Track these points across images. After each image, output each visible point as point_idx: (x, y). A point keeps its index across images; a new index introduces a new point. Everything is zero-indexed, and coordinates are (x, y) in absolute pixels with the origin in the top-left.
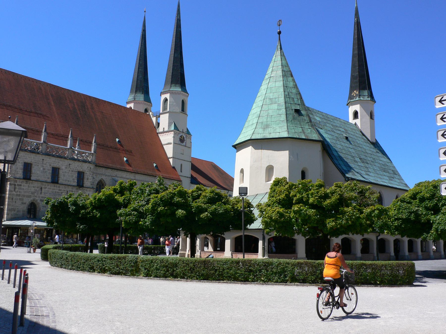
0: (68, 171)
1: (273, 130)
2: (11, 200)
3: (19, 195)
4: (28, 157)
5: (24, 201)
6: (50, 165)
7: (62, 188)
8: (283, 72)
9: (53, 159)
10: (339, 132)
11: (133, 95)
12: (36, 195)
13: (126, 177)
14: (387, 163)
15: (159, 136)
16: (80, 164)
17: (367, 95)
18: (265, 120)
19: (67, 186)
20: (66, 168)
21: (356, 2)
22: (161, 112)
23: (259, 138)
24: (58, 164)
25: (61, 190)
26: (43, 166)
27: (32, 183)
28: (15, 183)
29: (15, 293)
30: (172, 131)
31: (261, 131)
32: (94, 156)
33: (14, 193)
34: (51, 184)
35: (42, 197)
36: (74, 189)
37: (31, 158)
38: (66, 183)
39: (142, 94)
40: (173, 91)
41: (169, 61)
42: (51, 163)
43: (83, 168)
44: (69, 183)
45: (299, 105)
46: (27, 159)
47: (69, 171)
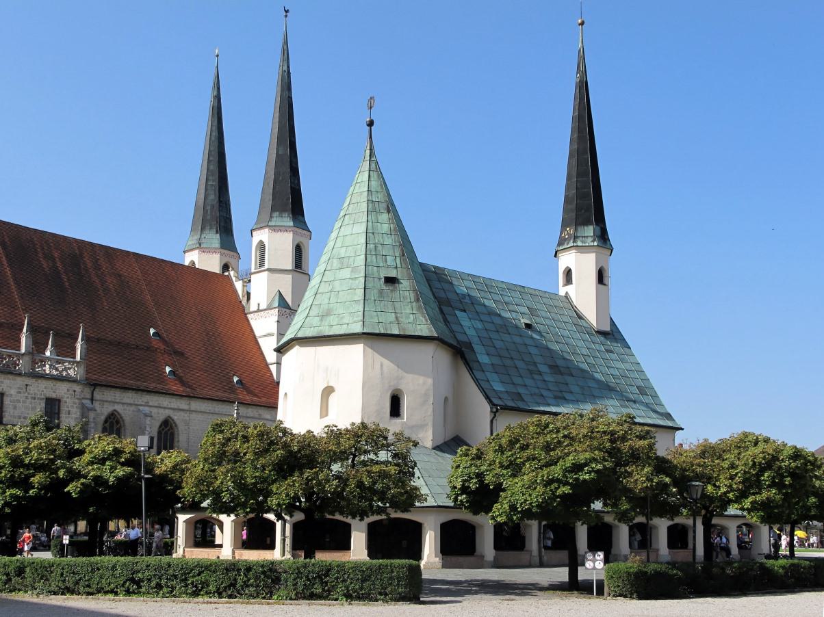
1: (337, 319)
8: (370, 205)
13: (169, 406)
16: (50, 383)
17: (592, 237)
18: (326, 301)
20: (20, 393)
21: (581, 39)
22: (253, 270)
31: (316, 321)
32: (82, 367)
39: (217, 233)
41: (268, 163)
43: (57, 391)
45: (396, 268)
47: (27, 398)
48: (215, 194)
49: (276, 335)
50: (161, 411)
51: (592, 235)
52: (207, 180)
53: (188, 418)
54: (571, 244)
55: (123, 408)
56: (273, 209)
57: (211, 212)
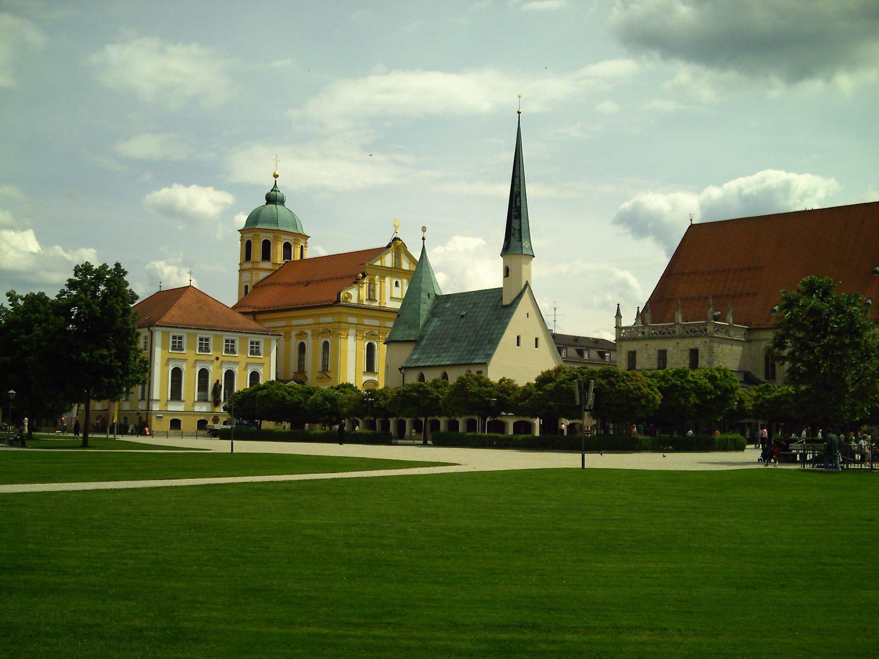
6: (655, 349)
9: (658, 342)
20: (674, 349)
26: (647, 352)
47: (678, 351)
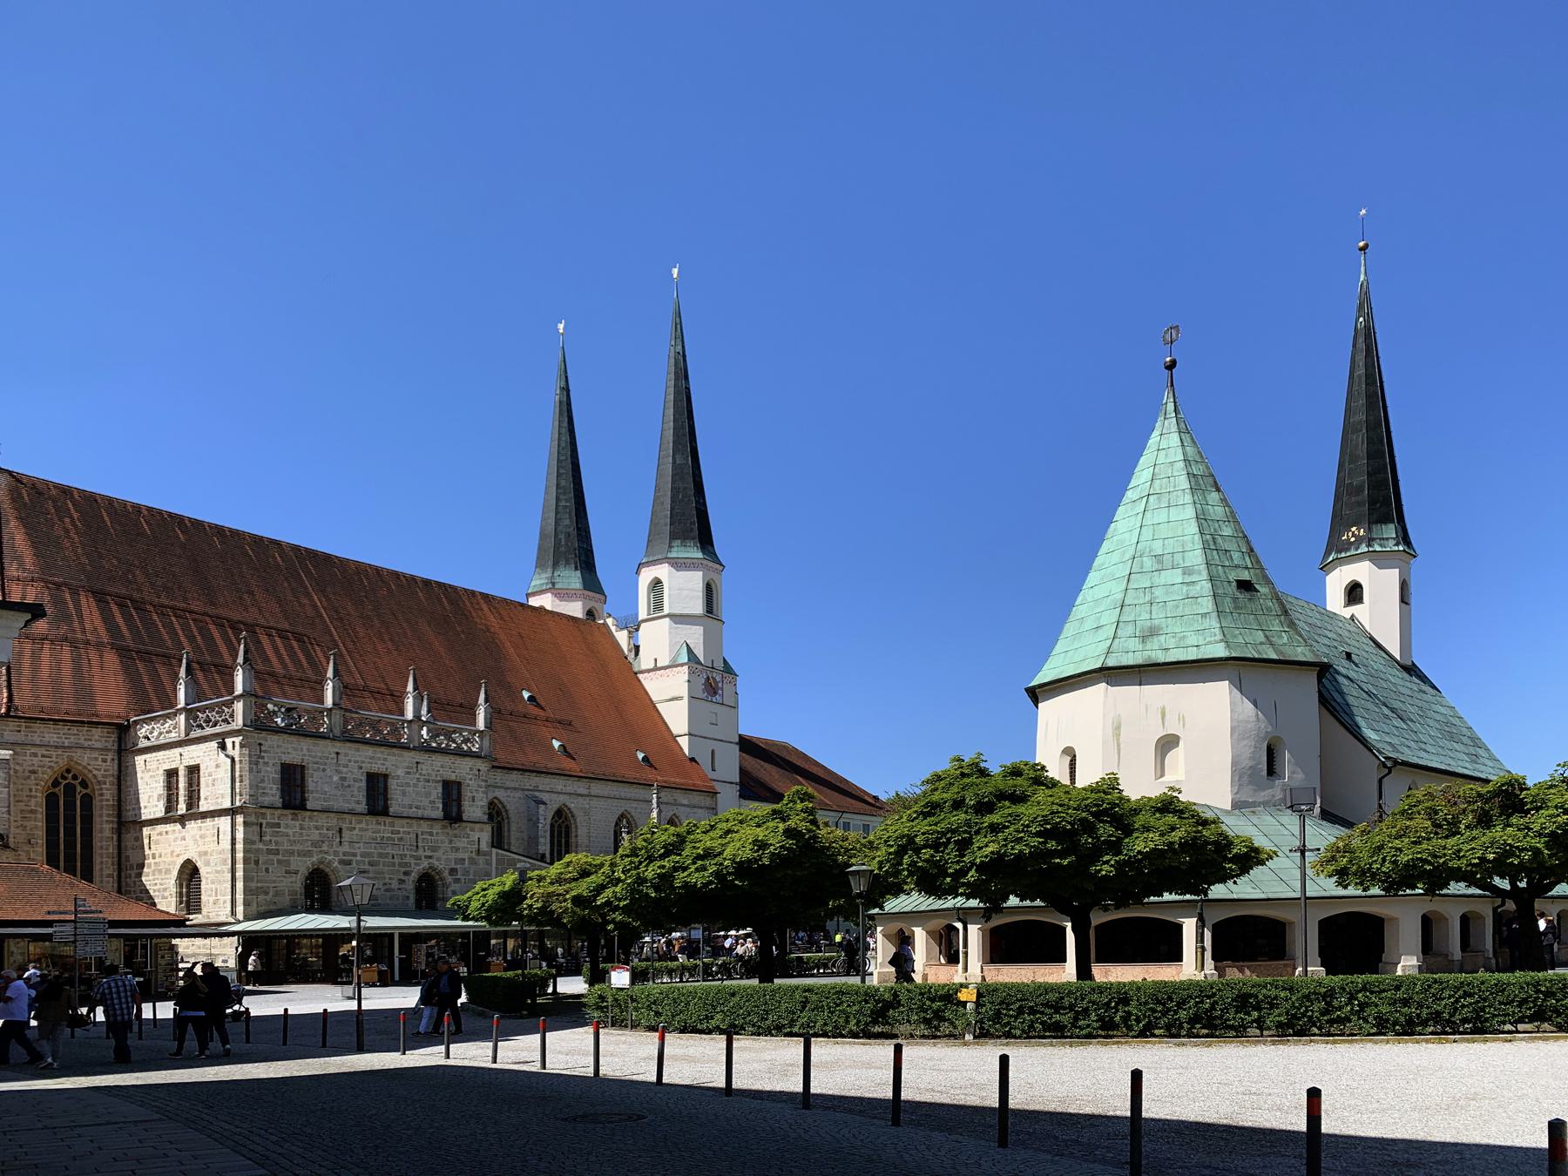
0: (415, 782)
2: (252, 865)
3: (277, 852)
4: (292, 747)
5: (293, 867)
7: (401, 825)
8: (1192, 479)
9: (369, 751)
10: (1326, 641)
11: (549, 574)
12: (325, 848)
14: (1450, 718)
15: (642, 680)
16: (448, 760)
19: (414, 821)
20: (409, 773)
23: (1131, 662)
24: (383, 764)
25: (399, 832)
27: (310, 818)
28: (260, 821)
29: (1547, 1124)
30: (682, 665)
31: (1134, 644)
32: (488, 738)
33: (261, 846)
34: (368, 817)
35: (345, 854)
36: (437, 828)
37: (302, 750)
38: (413, 812)
39: (576, 569)
40: (679, 560)
42: (363, 762)
43: (457, 771)
44: (420, 813)
45: (1247, 568)
46: (288, 753)
48: (570, 518)
49: (685, 702)
50: (554, 796)
51: (1394, 536)
52: (558, 499)
53: (588, 806)
54: (1364, 548)
55: (505, 795)
56: (673, 537)
57: (566, 541)
